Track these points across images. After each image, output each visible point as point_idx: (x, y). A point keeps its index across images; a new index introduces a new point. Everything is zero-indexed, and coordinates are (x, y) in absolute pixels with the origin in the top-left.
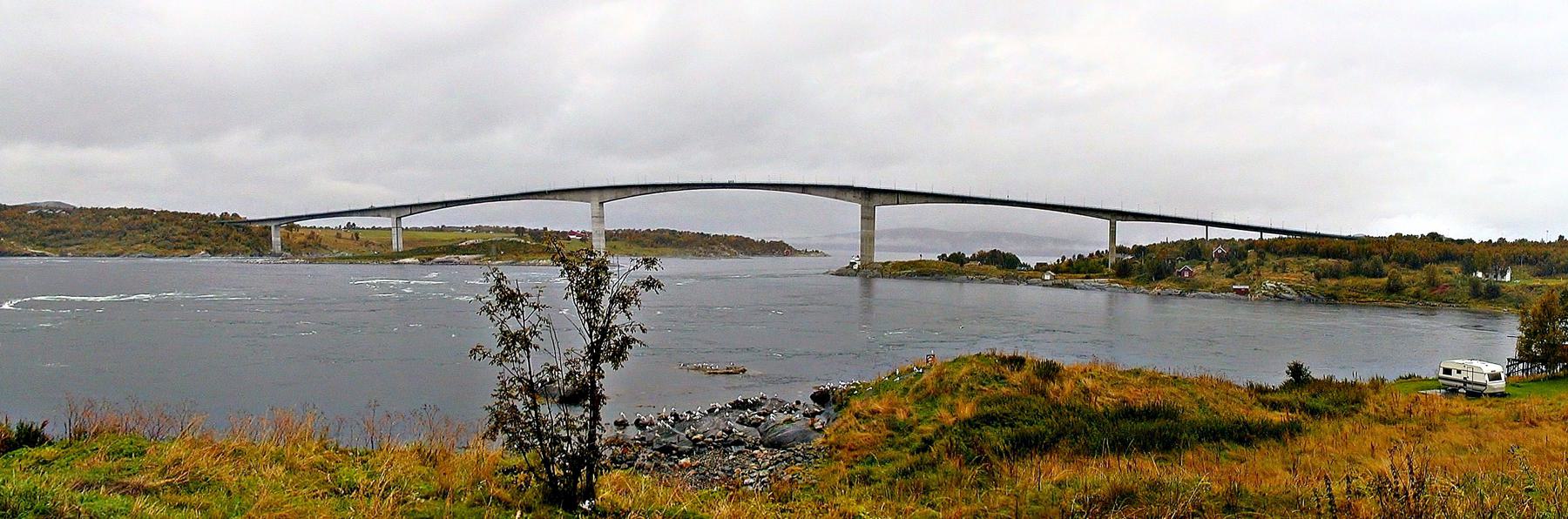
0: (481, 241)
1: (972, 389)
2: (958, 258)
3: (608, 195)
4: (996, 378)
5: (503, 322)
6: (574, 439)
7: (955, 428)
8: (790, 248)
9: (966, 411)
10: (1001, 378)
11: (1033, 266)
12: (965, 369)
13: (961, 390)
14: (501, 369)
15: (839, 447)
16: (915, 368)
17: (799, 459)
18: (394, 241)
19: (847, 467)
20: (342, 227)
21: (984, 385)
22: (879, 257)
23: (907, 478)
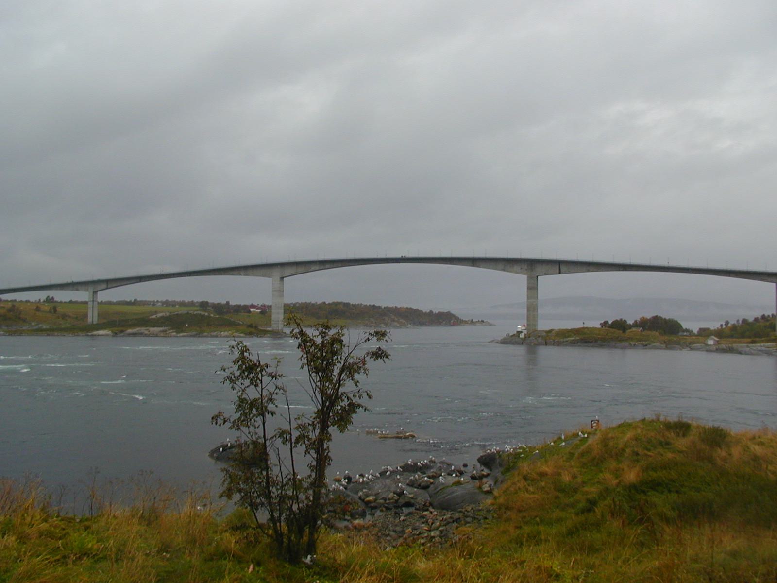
0: (168, 314)
1: (637, 454)
2: (620, 325)
3: (288, 271)
4: (661, 444)
5: (243, 391)
6: (302, 496)
7: (618, 490)
8: (457, 318)
9: (631, 476)
10: (666, 444)
11: (695, 331)
12: (629, 435)
13: (626, 455)
14: (238, 433)
15: (507, 508)
16: (580, 433)
17: (469, 519)
18: (90, 314)
19: (517, 527)
20: (42, 301)
21: (649, 450)
22: (543, 325)
23: (572, 537)
